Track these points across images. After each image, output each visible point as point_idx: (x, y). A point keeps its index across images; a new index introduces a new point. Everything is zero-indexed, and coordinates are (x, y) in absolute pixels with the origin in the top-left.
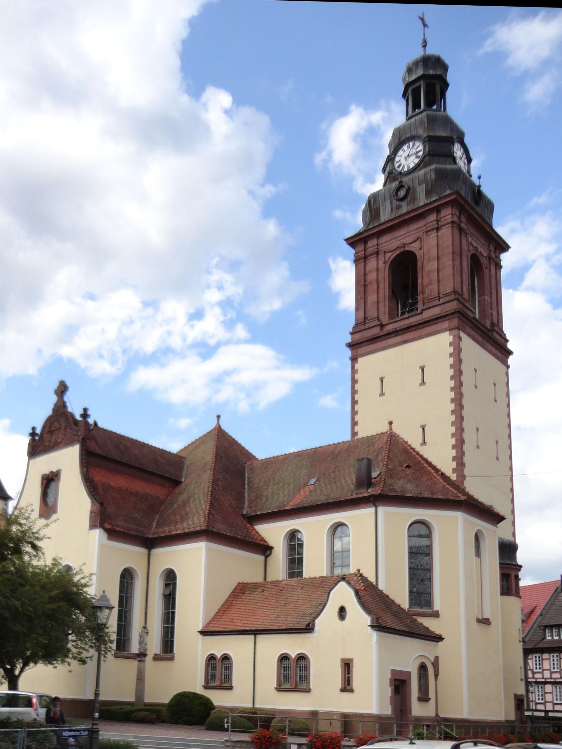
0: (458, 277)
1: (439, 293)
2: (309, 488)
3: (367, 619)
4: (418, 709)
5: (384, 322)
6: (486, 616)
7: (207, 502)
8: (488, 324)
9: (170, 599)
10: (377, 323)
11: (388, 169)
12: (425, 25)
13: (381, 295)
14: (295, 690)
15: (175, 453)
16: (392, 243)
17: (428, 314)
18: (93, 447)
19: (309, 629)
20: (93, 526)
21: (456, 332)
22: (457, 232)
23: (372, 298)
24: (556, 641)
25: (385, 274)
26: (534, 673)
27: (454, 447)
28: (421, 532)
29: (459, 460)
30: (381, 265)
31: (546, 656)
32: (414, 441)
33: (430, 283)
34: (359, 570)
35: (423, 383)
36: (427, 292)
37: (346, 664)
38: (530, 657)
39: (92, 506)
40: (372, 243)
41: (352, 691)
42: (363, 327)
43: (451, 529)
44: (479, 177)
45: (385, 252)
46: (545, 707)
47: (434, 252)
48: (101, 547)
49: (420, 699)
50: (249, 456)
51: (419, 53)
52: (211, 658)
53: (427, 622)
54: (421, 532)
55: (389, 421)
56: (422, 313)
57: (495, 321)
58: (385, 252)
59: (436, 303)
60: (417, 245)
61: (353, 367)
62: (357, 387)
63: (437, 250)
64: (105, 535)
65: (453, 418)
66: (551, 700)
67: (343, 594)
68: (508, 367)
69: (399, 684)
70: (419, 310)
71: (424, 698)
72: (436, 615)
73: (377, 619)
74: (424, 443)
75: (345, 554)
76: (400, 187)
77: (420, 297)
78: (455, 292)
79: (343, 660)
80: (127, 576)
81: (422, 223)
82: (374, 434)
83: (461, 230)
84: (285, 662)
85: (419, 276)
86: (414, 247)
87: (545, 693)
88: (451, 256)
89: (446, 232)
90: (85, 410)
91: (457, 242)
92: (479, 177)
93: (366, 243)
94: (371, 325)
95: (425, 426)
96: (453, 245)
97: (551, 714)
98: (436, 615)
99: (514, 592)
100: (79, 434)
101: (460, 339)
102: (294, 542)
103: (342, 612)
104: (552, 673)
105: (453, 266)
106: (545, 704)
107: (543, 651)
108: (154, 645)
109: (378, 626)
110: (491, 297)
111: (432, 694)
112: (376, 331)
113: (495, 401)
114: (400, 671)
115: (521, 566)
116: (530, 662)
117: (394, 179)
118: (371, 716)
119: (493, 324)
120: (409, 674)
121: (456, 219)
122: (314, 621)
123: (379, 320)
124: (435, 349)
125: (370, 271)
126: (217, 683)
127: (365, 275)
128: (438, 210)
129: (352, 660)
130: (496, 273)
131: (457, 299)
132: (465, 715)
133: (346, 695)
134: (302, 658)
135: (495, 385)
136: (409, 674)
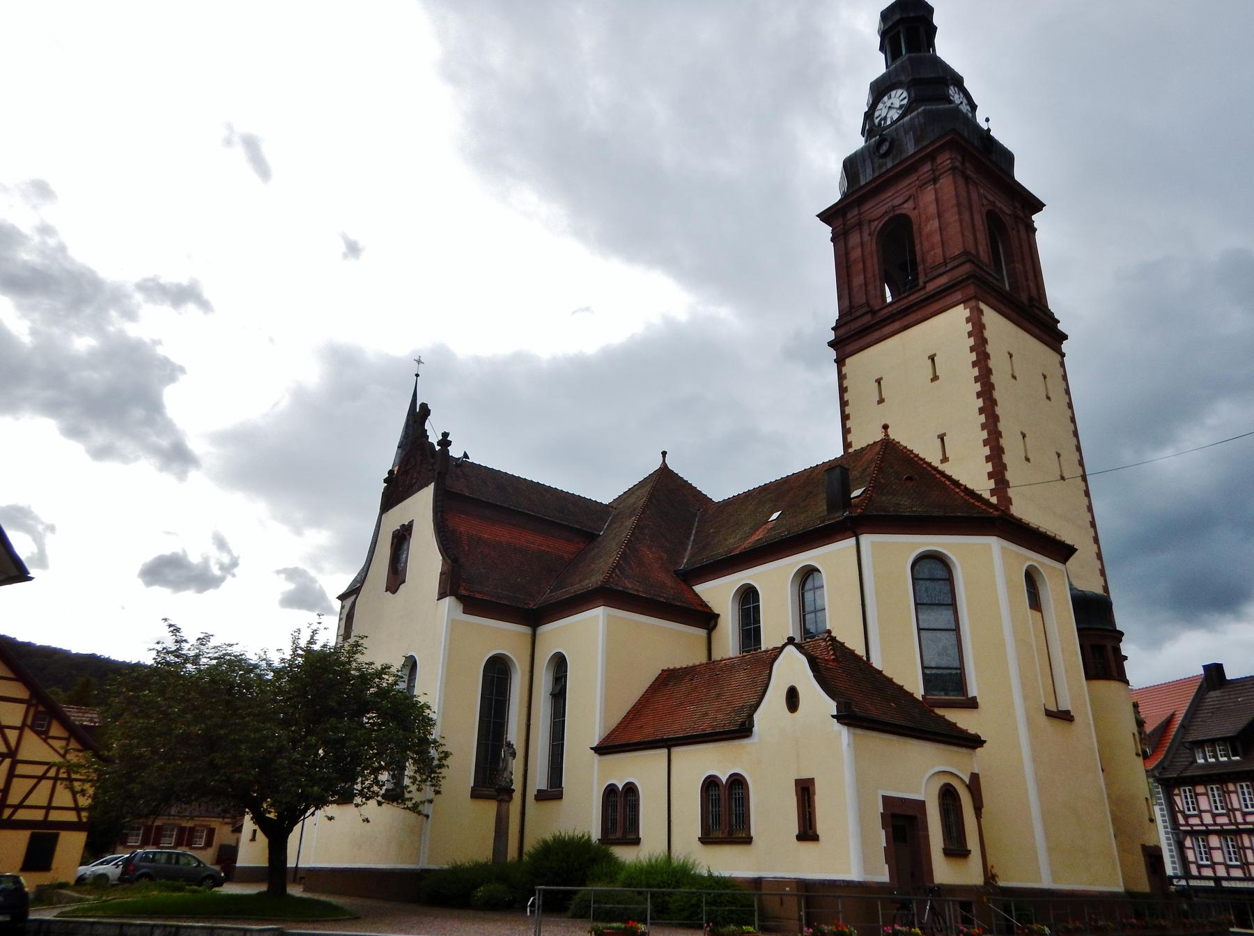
0: (968, 234)
2: (769, 526)
3: (831, 706)
4: (944, 872)
6: (1064, 706)
8: (1024, 298)
9: (559, 696)
13: (869, 275)
16: (878, 209)
17: (931, 287)
18: (460, 487)
19: (744, 730)
20: (442, 595)
21: (973, 303)
22: (961, 182)
23: (858, 281)
25: (872, 247)
26: (1186, 817)
27: (988, 459)
28: (933, 578)
29: (998, 474)
30: (866, 238)
31: (1200, 789)
32: (930, 454)
33: (932, 248)
35: (935, 378)
36: (929, 260)
38: (1176, 791)
40: (852, 215)
41: (815, 838)
42: (849, 318)
43: (982, 562)
44: (987, 120)
45: (870, 221)
46: (1215, 872)
47: (932, 209)
48: (453, 624)
52: (611, 791)
53: (962, 719)
54: (933, 578)
56: (924, 287)
57: (1034, 293)
58: (870, 221)
59: (943, 270)
60: (910, 204)
62: (846, 397)
63: (938, 212)
65: (982, 418)
66: (1221, 860)
67: (792, 669)
68: (1063, 355)
69: (901, 822)
70: (921, 284)
71: (956, 850)
72: (972, 704)
74: (945, 459)
75: (819, 614)
77: (920, 268)
78: (966, 253)
79: (798, 782)
80: (497, 673)
81: (914, 177)
82: (864, 445)
83: (967, 179)
84: (713, 792)
85: (917, 242)
86: (907, 208)
87: (1211, 849)
88: (955, 209)
89: (946, 182)
90: (445, 435)
91: (963, 192)
92: (987, 120)
93: (844, 215)
94: (859, 313)
95: (944, 434)
96: (957, 196)
97: (1225, 884)
98: (972, 704)
99: (1115, 674)
101: (981, 312)
102: (748, 598)
103: (792, 699)
104: (1214, 816)
105: (961, 221)
106: (1213, 866)
107: (1194, 781)
108: (539, 779)
109: (846, 717)
110: (1024, 265)
111: (972, 843)
114: (902, 799)
116: (1177, 799)
118: (849, 885)
119: (1031, 299)
120: (921, 805)
121: (958, 164)
122: (750, 717)
125: (853, 248)
126: (619, 834)
128: (932, 157)
130: (1028, 237)
131: (970, 261)
132: (1045, 881)
133: (808, 846)
134: (737, 781)
135: (1045, 377)
136: (921, 805)
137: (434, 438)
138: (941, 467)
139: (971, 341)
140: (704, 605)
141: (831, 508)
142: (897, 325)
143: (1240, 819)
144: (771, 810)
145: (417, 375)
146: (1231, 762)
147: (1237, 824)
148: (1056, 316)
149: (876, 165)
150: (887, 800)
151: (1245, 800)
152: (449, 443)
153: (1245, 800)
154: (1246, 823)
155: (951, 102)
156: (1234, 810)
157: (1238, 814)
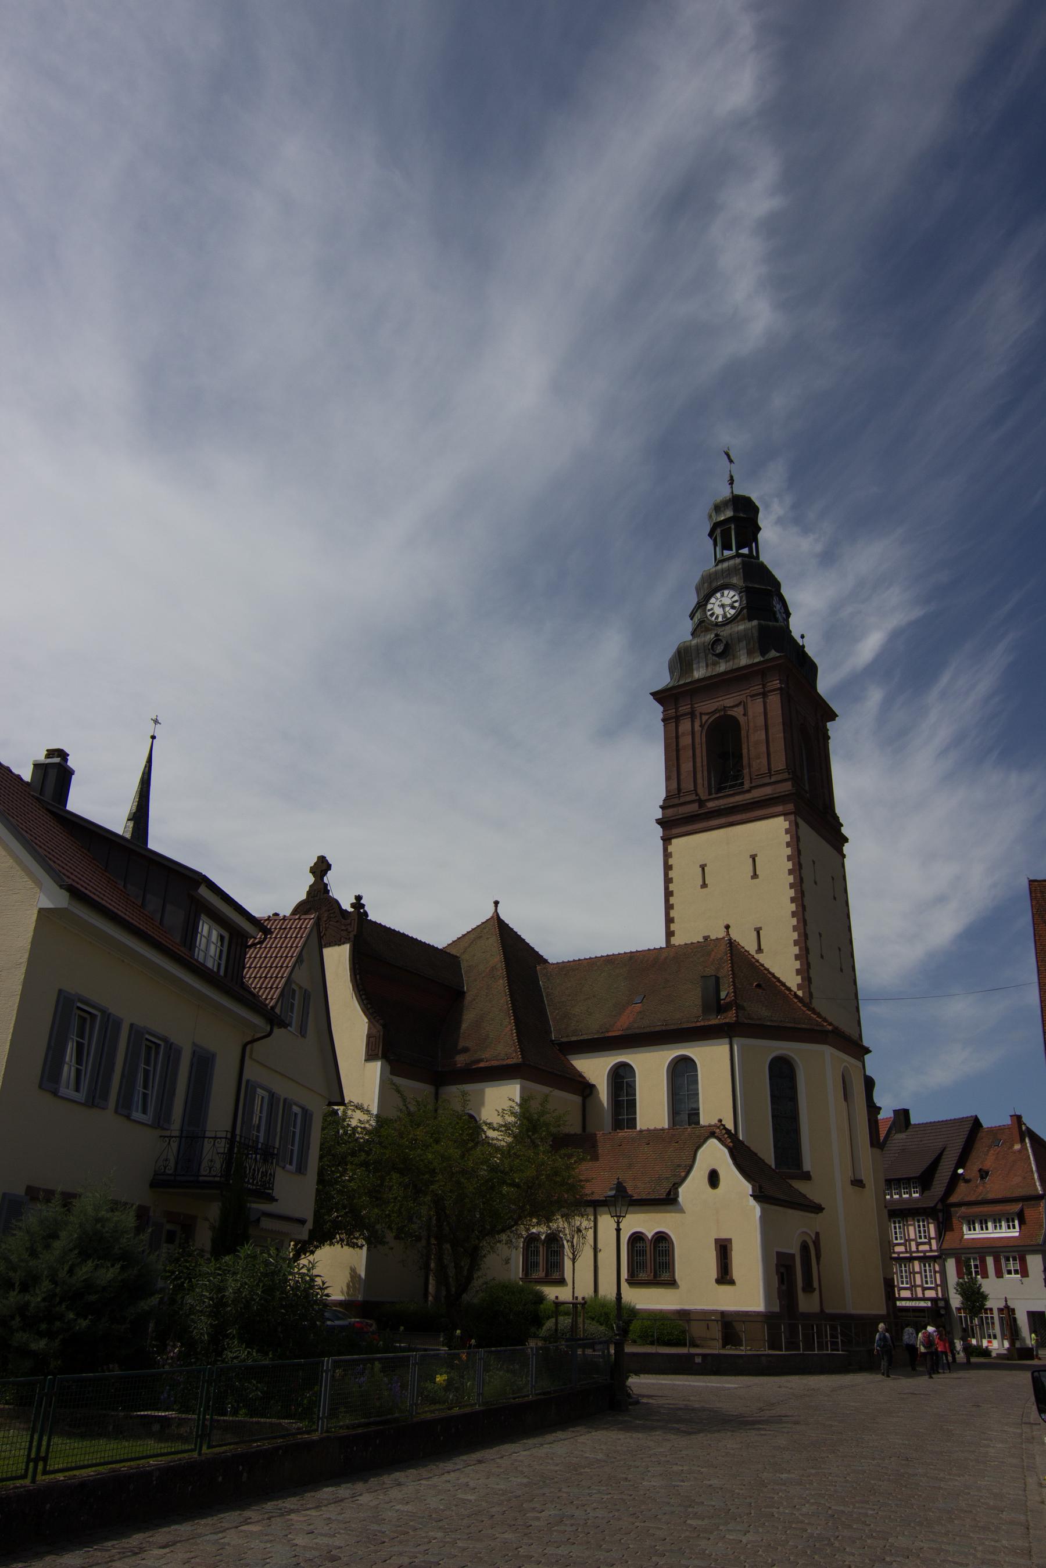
1: (769, 769)
3: (747, 1187)
4: (807, 1304)
5: (703, 798)
7: (510, 1024)
10: (694, 797)
11: (698, 616)
12: (731, 461)
14: (655, 1282)
15: (440, 947)
16: (708, 706)
19: (669, 1200)
20: (370, 1057)
21: (792, 817)
23: (687, 767)
24: (897, 1200)
25: (701, 739)
28: (783, 1075)
29: (805, 972)
30: (697, 727)
34: (720, 1121)
35: (755, 876)
37: (721, 1246)
39: (369, 1028)
41: (732, 1282)
42: (676, 801)
45: (701, 714)
49: (804, 1290)
50: (541, 960)
51: (725, 493)
54: (783, 1075)
55: (726, 923)
56: (749, 791)
59: (767, 780)
60: (740, 709)
61: (665, 849)
63: (761, 718)
64: (388, 1068)
68: (844, 856)
71: (808, 1288)
72: (807, 1176)
73: (760, 1187)
74: (760, 950)
76: (717, 640)
77: (746, 771)
79: (717, 1241)
85: (744, 746)
86: (737, 712)
89: (775, 701)
90: (359, 898)
92: (802, 637)
100: (350, 929)
102: (622, 1079)
103: (714, 1179)
111: (816, 1284)
112: (694, 808)
113: (835, 898)
115: (880, 1108)
117: (707, 630)
120: (793, 1256)
123: (697, 795)
124: (770, 835)
127: (677, 737)
129: (729, 1241)
134: (662, 1238)
137: (346, 905)
138: (756, 956)
139: (789, 851)
140: (581, 1075)
141: (706, 1009)
142: (722, 821)
143: (914, 1248)
144: (694, 1262)
145: (153, 737)
146: (911, 1199)
147: (911, 1252)
148: (841, 821)
149: (710, 662)
150: (778, 1253)
151: (920, 1232)
152: (363, 906)
153: (920, 1232)
154: (918, 1251)
155: (776, 620)
156: (910, 1240)
157: (913, 1244)
